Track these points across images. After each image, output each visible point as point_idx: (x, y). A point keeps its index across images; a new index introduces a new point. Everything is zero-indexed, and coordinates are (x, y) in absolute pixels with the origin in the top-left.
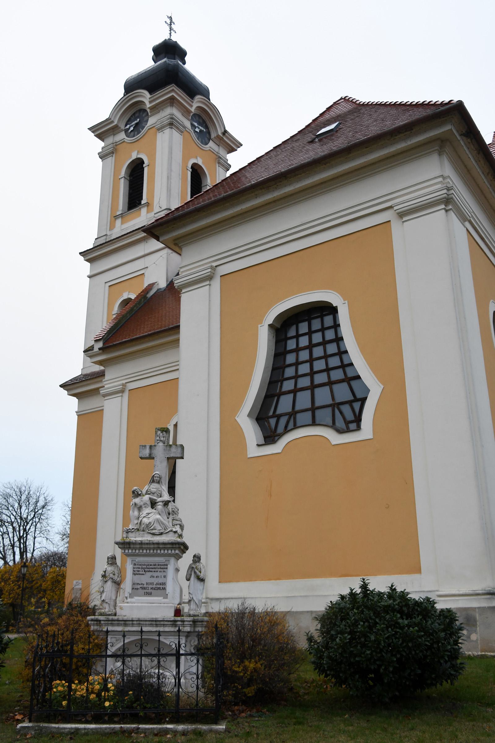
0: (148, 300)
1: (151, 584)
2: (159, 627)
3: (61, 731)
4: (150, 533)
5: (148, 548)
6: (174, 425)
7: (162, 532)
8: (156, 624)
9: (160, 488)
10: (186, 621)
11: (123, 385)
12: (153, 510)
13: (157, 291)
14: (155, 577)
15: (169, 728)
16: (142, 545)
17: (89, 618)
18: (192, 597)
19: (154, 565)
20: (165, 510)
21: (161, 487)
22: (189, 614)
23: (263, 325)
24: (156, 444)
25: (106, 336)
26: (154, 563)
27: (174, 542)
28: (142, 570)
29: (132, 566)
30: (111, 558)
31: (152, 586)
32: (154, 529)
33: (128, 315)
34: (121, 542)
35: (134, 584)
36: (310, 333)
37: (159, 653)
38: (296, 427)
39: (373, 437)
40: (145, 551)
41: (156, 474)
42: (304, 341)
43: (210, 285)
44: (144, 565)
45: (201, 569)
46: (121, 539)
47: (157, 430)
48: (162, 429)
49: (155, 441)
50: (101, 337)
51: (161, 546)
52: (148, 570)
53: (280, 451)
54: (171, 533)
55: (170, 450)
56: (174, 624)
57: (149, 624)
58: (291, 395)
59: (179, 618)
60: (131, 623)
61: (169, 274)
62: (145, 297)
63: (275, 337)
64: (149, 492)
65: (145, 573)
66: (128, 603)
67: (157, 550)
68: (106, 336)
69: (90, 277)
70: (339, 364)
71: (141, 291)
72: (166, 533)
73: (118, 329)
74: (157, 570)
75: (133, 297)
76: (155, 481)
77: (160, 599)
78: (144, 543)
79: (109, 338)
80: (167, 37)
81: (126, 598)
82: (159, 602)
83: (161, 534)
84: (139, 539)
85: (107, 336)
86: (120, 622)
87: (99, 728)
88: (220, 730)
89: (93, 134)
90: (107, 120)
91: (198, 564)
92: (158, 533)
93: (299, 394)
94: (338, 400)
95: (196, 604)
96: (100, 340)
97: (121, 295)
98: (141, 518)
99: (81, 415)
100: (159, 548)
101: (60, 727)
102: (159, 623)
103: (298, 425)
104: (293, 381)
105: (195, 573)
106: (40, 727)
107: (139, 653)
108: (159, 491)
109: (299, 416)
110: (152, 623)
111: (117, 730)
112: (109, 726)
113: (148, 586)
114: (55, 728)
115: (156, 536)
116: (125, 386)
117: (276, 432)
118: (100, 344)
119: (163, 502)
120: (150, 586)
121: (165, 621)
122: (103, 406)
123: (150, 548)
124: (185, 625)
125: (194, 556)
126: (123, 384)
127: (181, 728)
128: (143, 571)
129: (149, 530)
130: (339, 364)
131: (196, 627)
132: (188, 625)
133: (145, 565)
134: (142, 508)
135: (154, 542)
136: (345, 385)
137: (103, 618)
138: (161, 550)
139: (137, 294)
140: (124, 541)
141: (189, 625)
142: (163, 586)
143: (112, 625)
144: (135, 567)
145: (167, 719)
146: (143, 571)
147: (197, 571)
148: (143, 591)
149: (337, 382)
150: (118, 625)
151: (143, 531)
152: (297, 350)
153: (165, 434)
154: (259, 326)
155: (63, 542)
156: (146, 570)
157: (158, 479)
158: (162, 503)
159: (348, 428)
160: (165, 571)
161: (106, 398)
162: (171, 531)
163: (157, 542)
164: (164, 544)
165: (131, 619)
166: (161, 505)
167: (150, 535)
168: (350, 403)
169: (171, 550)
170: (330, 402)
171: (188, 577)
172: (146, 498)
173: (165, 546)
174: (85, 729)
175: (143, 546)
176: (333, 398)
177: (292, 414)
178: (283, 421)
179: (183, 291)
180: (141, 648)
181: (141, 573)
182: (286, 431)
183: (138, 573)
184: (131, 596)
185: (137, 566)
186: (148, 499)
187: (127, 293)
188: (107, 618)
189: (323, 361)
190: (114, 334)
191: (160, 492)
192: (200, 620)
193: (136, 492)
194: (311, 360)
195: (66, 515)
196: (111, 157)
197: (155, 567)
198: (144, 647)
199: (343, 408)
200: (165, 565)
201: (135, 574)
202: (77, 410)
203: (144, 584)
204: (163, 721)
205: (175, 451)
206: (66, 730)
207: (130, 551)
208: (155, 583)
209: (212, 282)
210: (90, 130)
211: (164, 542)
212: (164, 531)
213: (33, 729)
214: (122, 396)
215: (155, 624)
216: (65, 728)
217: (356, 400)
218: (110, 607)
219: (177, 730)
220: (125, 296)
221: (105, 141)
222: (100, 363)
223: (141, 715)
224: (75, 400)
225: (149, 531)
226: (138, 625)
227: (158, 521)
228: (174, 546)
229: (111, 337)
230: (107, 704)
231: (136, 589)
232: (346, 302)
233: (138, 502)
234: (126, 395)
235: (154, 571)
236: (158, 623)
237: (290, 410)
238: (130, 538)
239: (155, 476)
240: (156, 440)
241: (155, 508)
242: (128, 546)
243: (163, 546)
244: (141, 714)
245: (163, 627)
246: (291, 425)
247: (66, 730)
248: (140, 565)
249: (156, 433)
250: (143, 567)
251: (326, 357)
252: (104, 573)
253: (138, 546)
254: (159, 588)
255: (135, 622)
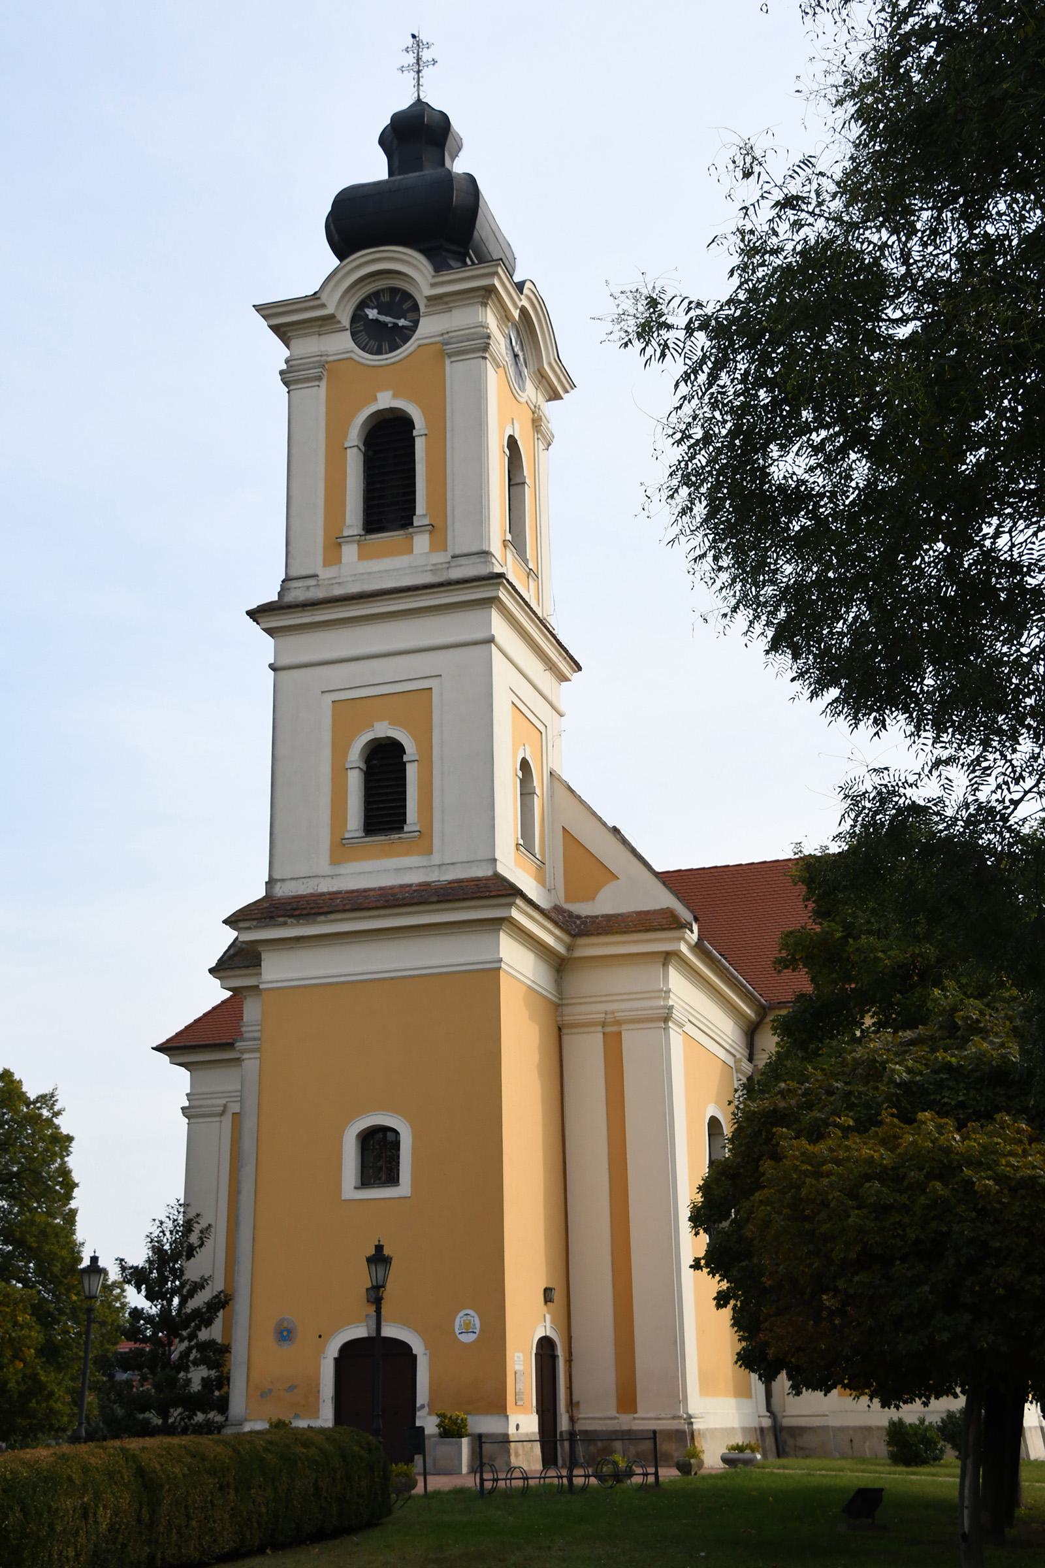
80: (404, 102)
89: (265, 323)
90: (306, 299)
196: (317, 388)
210: (257, 310)
221: (293, 343)
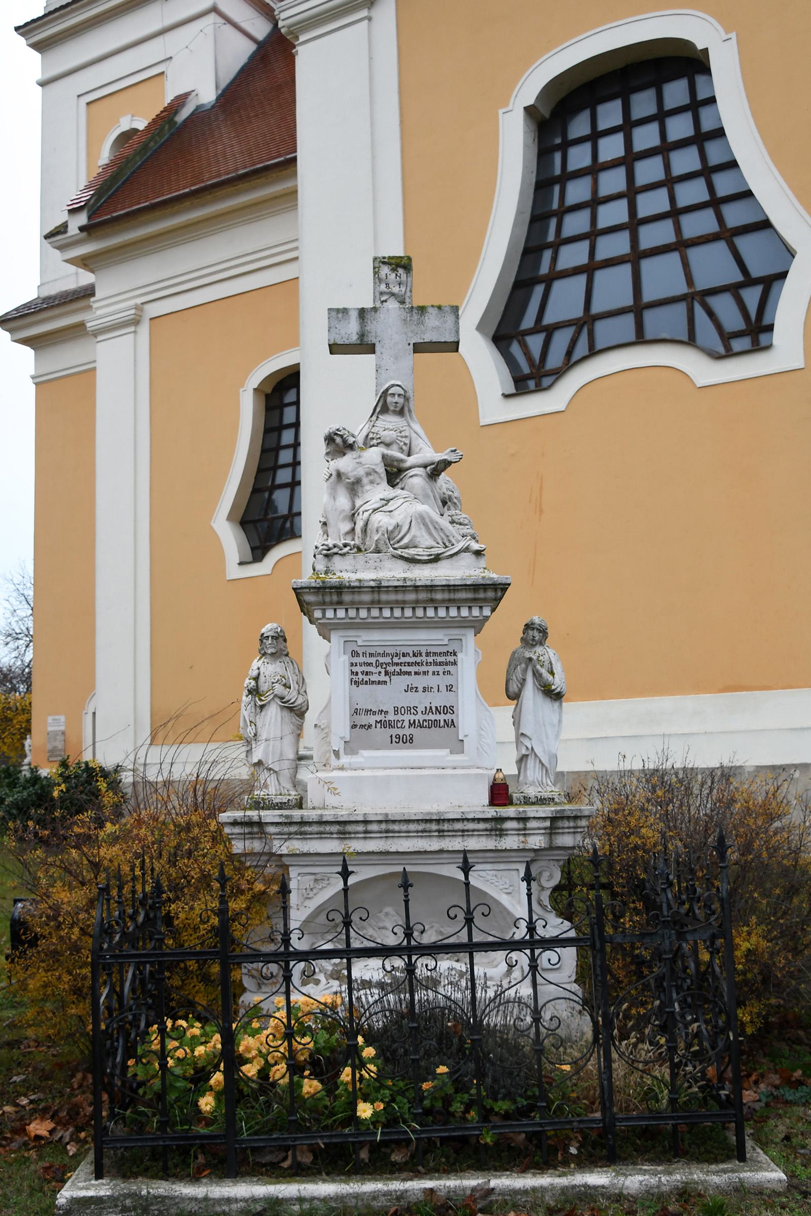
0: (178, 128)
1: (409, 710)
2: (448, 839)
3: (218, 1209)
4: (402, 558)
5: (397, 602)
6: (255, 389)
7: (439, 555)
8: (439, 831)
9: (407, 428)
10: (534, 818)
11: (136, 307)
12: (398, 491)
13: (196, 110)
14: (420, 689)
15: (595, 1188)
16: (379, 592)
17: (224, 817)
18: (530, 747)
19: (414, 655)
20: (432, 491)
21: (409, 425)
22: (524, 797)
23: (510, 108)
24: (378, 304)
25: (92, 201)
26: (416, 649)
27: (481, 582)
28: (379, 669)
29: (345, 659)
30: (272, 637)
31: (412, 718)
32: (413, 545)
33: (138, 158)
34: (313, 585)
35: (356, 712)
36: (628, 126)
37: (532, 936)
38: (594, 352)
39: (806, 363)
40: (387, 613)
41: (393, 386)
42: (611, 148)
43: (369, 19)
44: (384, 655)
45: (551, 663)
46: (311, 578)
47: (377, 265)
48: (393, 261)
49: (375, 297)
50: (82, 204)
51: (439, 596)
52: (397, 669)
53: (561, 407)
54: (468, 558)
55: (420, 323)
56: (496, 830)
57: (417, 832)
58: (582, 279)
59: (510, 811)
60: (361, 828)
61: (220, 74)
62: (171, 122)
63: (536, 140)
64: (375, 442)
65: (387, 679)
66: (342, 769)
67: (425, 608)
68: (92, 201)
69: (42, 84)
70: (705, 197)
71: (162, 109)
72: (452, 556)
73: (118, 188)
74: (424, 668)
75: (141, 125)
76: (392, 408)
77: (442, 754)
78: (387, 587)
79: (101, 206)
81: (337, 754)
82: (438, 765)
83: (436, 559)
84: (368, 575)
85: (97, 201)
86: (328, 828)
87: (349, 1195)
88: (769, 1185)
91: (539, 650)
92: (427, 558)
93: (600, 276)
94: (702, 284)
95: (543, 764)
96: (80, 209)
97: (116, 122)
98: (366, 514)
99: (41, 384)
100: (432, 600)
101: (211, 1195)
102: (451, 828)
103: (599, 346)
104: (585, 245)
105: (537, 675)
106: (141, 1197)
107: (463, 938)
108: (406, 437)
109: (601, 327)
110: (428, 826)
111: (413, 1199)
112: (386, 1188)
113: (400, 717)
114: (195, 1199)
115: (418, 566)
116: (142, 310)
117: (543, 367)
118: (82, 219)
119: (425, 467)
120: (407, 718)
121: (468, 820)
122: (95, 361)
123: (404, 602)
124: (530, 829)
125: (529, 627)
126: (136, 305)
127: (637, 1185)
128: (383, 671)
129: (395, 549)
130: (705, 197)
131: (556, 833)
132: (539, 829)
133: (388, 655)
134: (362, 487)
135: (419, 583)
136: (720, 249)
137: (274, 816)
138: (436, 608)
139: (150, 120)
140: (323, 582)
141: (543, 831)
142: (448, 717)
143: (303, 836)
144: (356, 660)
145: (573, 1151)
146: (383, 673)
147: (544, 671)
148: (384, 734)
149: (700, 240)
150: (321, 836)
151: (378, 551)
152: (595, 169)
153: (404, 277)
154: (501, 111)
155: (6, 649)
156: (391, 669)
157: (401, 401)
158: (421, 469)
159: (728, 348)
160: (449, 672)
161: (100, 338)
162: (467, 549)
163: (429, 583)
164: (450, 588)
165: (361, 818)
166: (421, 476)
167: (401, 563)
168: (734, 289)
169: (470, 608)
170: (681, 288)
171: (514, 687)
172: (373, 456)
173: (452, 596)
174: (301, 1200)
175: (384, 597)
176: (690, 280)
177: (585, 323)
178: (561, 340)
179: (302, 38)
180: (469, 921)
181: (374, 678)
182: (569, 363)
183: (366, 678)
184: (350, 747)
185: (361, 659)
186: (380, 459)
187: (129, 117)
188: (287, 817)
189: (663, 193)
190: (110, 197)
191: (407, 442)
192: (568, 814)
193: (338, 440)
194: (631, 193)
195: (11, 599)
197: (418, 659)
198: (478, 920)
199: (715, 302)
200: (446, 654)
201: (357, 683)
202: (33, 373)
203: (386, 712)
204: (560, 1157)
205: (437, 323)
206: (234, 1206)
207: (341, 613)
208: (421, 708)
209: (377, 13)
211: (452, 583)
212: (444, 550)
213: (116, 1206)
214: (135, 332)
215: (436, 831)
216: (229, 1201)
217: (749, 281)
218: (280, 784)
219: (625, 1192)
220: (125, 125)
222: (84, 262)
223: (486, 1144)
224: (28, 353)
225: (399, 552)
226: (384, 835)
227: (423, 520)
228: (481, 595)
229: (104, 202)
230: (365, 1111)
231: (362, 726)
232: (733, 35)
233: (350, 469)
234: (144, 329)
235: (416, 673)
236: (446, 826)
237: (578, 312)
238: (338, 574)
239: (390, 391)
240: (377, 294)
241: (400, 486)
242: (335, 598)
243: (446, 596)
244: (488, 1140)
245: (459, 839)
246: (582, 348)
247: (234, 1206)
248: (371, 655)
249: (375, 273)
250: (382, 660)
251: (670, 182)
252: (253, 683)
253: (367, 598)
254: (435, 724)
255: (374, 827)
